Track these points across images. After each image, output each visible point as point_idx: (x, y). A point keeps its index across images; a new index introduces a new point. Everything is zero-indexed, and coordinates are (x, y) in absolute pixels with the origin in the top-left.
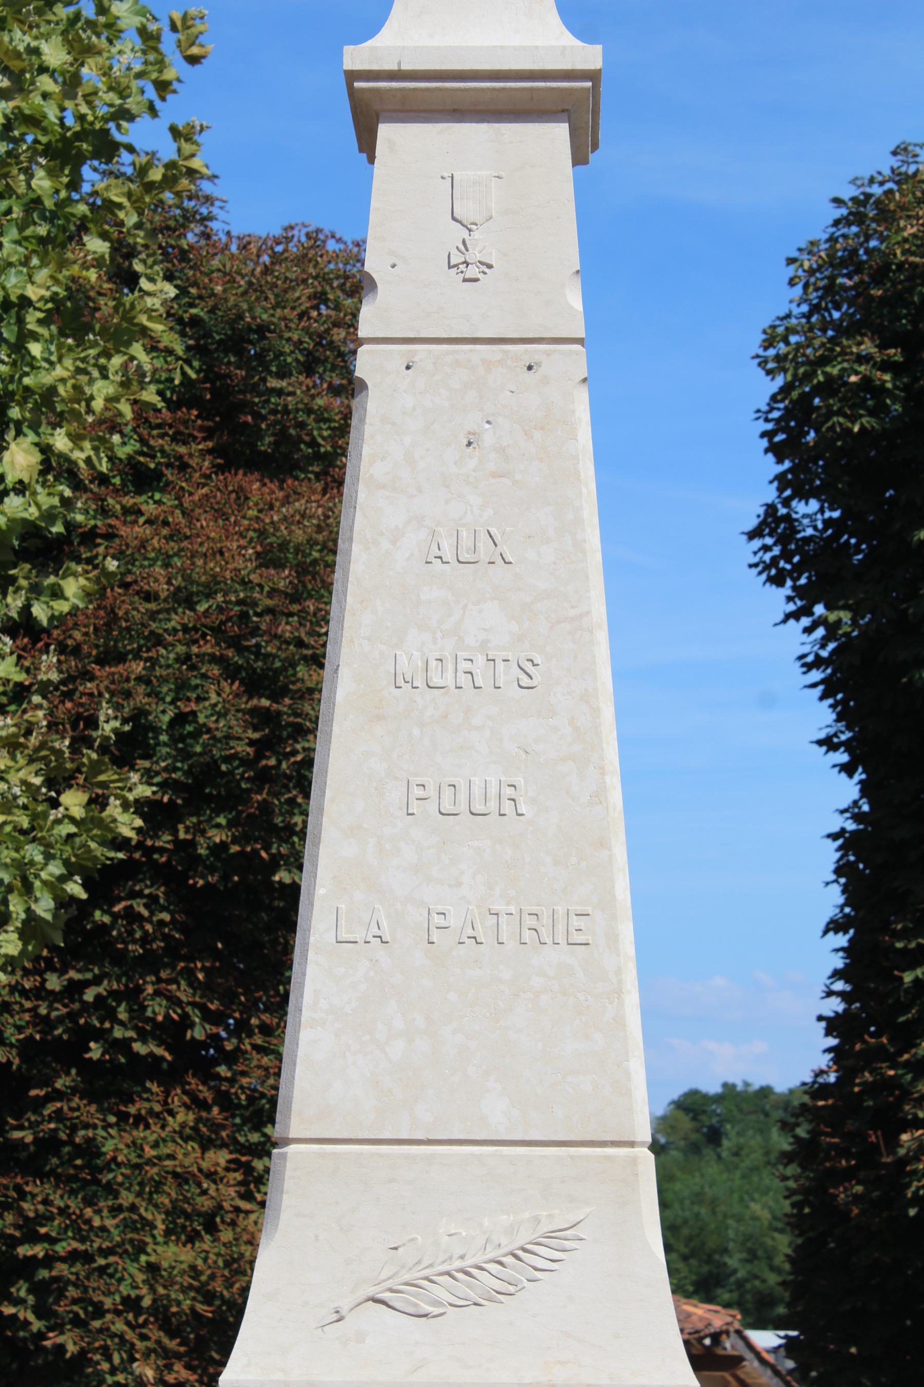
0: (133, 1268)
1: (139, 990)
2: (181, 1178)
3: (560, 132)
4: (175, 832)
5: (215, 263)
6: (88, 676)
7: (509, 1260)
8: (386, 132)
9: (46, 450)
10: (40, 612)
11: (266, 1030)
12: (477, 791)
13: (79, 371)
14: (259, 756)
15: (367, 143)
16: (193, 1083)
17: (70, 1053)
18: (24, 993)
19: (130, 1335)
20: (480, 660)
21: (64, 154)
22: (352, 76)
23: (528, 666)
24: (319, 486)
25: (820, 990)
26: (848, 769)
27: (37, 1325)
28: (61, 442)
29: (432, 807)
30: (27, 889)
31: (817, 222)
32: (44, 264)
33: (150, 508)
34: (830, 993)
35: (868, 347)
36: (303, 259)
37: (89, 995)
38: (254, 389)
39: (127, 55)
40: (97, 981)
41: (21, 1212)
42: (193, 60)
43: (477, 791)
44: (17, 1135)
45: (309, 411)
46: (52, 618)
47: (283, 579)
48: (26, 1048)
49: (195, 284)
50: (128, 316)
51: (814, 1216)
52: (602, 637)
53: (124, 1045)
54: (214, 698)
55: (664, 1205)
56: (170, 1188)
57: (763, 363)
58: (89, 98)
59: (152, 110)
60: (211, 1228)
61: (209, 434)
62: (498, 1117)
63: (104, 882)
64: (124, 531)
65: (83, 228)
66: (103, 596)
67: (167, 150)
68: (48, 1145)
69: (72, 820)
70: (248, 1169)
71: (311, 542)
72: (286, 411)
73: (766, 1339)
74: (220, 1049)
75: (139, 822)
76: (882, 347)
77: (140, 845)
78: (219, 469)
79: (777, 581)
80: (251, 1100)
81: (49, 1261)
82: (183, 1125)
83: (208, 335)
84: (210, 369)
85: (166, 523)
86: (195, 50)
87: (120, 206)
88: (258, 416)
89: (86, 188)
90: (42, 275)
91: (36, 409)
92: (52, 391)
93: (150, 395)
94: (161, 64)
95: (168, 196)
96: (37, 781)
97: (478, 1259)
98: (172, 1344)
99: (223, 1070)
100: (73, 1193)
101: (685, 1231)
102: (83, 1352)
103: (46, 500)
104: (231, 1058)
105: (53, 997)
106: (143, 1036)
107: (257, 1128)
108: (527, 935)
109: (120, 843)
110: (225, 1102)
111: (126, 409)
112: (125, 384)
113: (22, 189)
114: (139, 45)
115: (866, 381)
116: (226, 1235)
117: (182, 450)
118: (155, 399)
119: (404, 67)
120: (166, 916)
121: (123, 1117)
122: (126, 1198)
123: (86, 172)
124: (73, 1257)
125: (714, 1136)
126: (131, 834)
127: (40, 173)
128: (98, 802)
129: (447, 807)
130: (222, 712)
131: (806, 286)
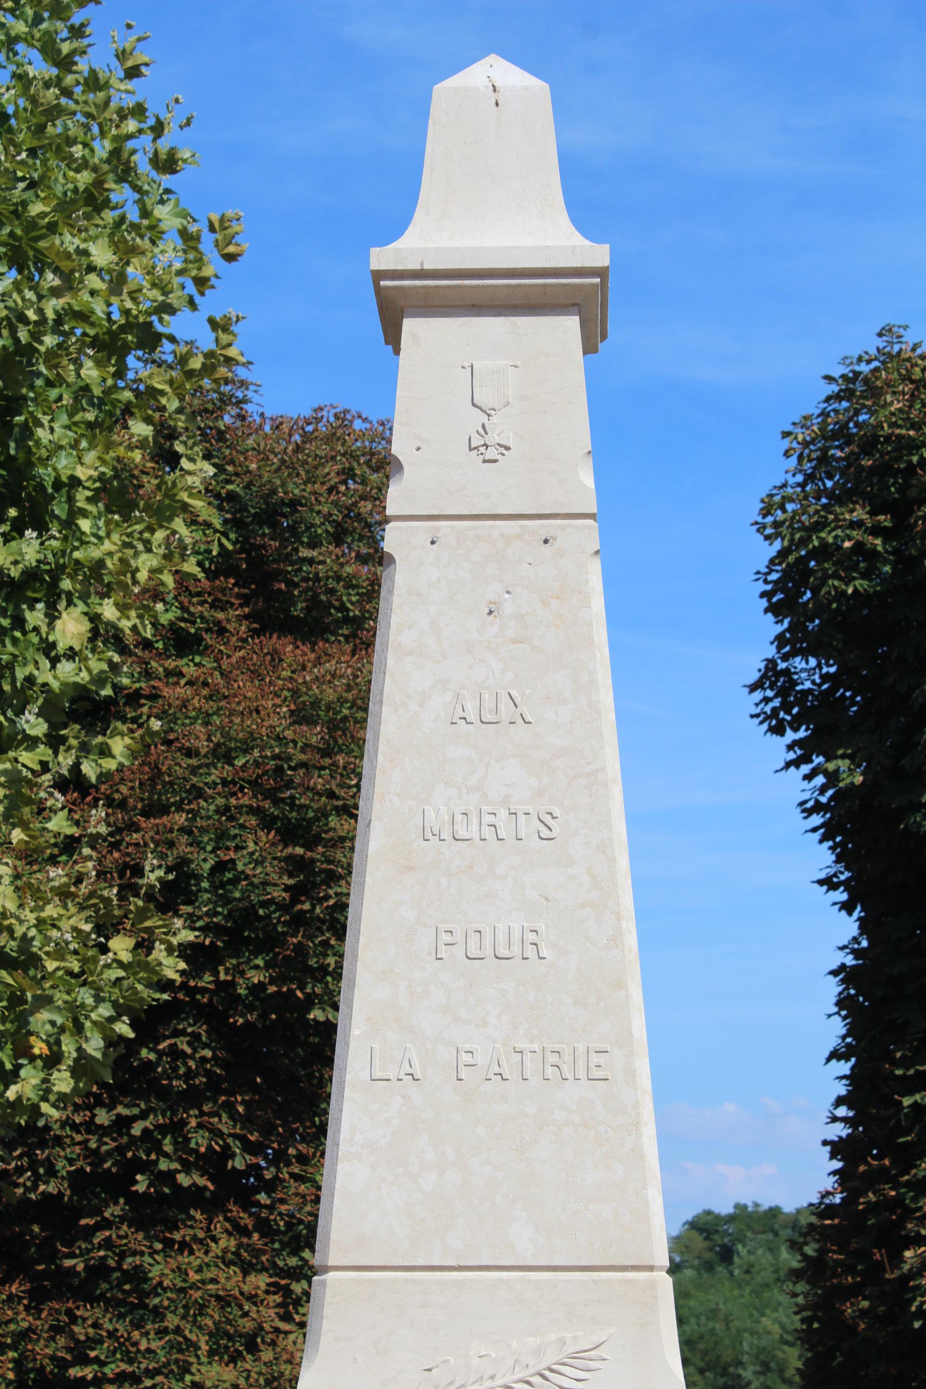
1: (183, 1123)
2: (224, 1301)
3: (571, 324)
4: (216, 973)
5: (250, 442)
6: (133, 827)
7: (537, 1380)
8: (410, 326)
9: (94, 618)
10: (89, 770)
11: (303, 1159)
12: (501, 937)
13: (126, 545)
14: (295, 900)
15: (393, 337)
16: (235, 1210)
17: (119, 1184)
18: (75, 1127)
20: (503, 813)
21: (110, 346)
22: (378, 276)
23: (548, 819)
24: (348, 648)
25: (824, 1115)
26: (847, 907)
28: (109, 611)
29: (459, 952)
30: (79, 1029)
31: (811, 397)
32: (92, 447)
33: (190, 671)
34: (834, 1119)
35: (860, 513)
36: (331, 438)
37: (136, 1130)
38: (287, 558)
39: (169, 254)
40: (143, 1116)
41: (72, 1336)
42: (230, 258)
43: (501, 937)
44: (68, 1263)
45: (338, 578)
46: (100, 776)
47: (315, 735)
48: (76, 1179)
49: (232, 462)
50: (170, 494)
52: (617, 791)
53: (170, 1176)
54: (251, 846)
55: (680, 1321)
56: (214, 1311)
57: (761, 528)
58: (134, 295)
59: (192, 303)
60: (252, 1348)
61: (246, 600)
62: (525, 1244)
63: (150, 1022)
64: (166, 692)
65: (128, 411)
66: (148, 754)
67: (206, 340)
68: (99, 1271)
69: (121, 964)
70: (286, 1291)
71: (342, 701)
72: (317, 579)
74: (260, 1178)
75: (182, 965)
76: (872, 513)
77: (184, 985)
78: (256, 633)
79: (778, 730)
80: (290, 1226)
82: (225, 1251)
83: (244, 509)
84: (246, 540)
85: (205, 684)
86: (231, 249)
87: (162, 393)
88: (291, 584)
89: (131, 375)
90: (91, 457)
91: (86, 581)
92: (101, 563)
93: (191, 566)
94: (199, 261)
95: (206, 383)
96: (87, 927)
99: (262, 1198)
100: (121, 1316)
101: (702, 1346)
103: (97, 666)
104: (270, 1186)
105: (103, 1131)
106: (187, 1168)
107: (295, 1252)
108: (550, 1072)
109: (165, 985)
110: (264, 1227)
111: (169, 580)
112: (168, 557)
113: (71, 378)
114: (180, 245)
115: (859, 547)
116: (267, 1355)
117: (221, 616)
118: (196, 570)
119: (427, 266)
120: (208, 1053)
121: (168, 1243)
122: (172, 1320)
123: (131, 361)
125: (726, 1255)
126: (176, 977)
127: (88, 364)
128: (144, 946)
129: (473, 951)
130: (259, 859)
131: (800, 458)
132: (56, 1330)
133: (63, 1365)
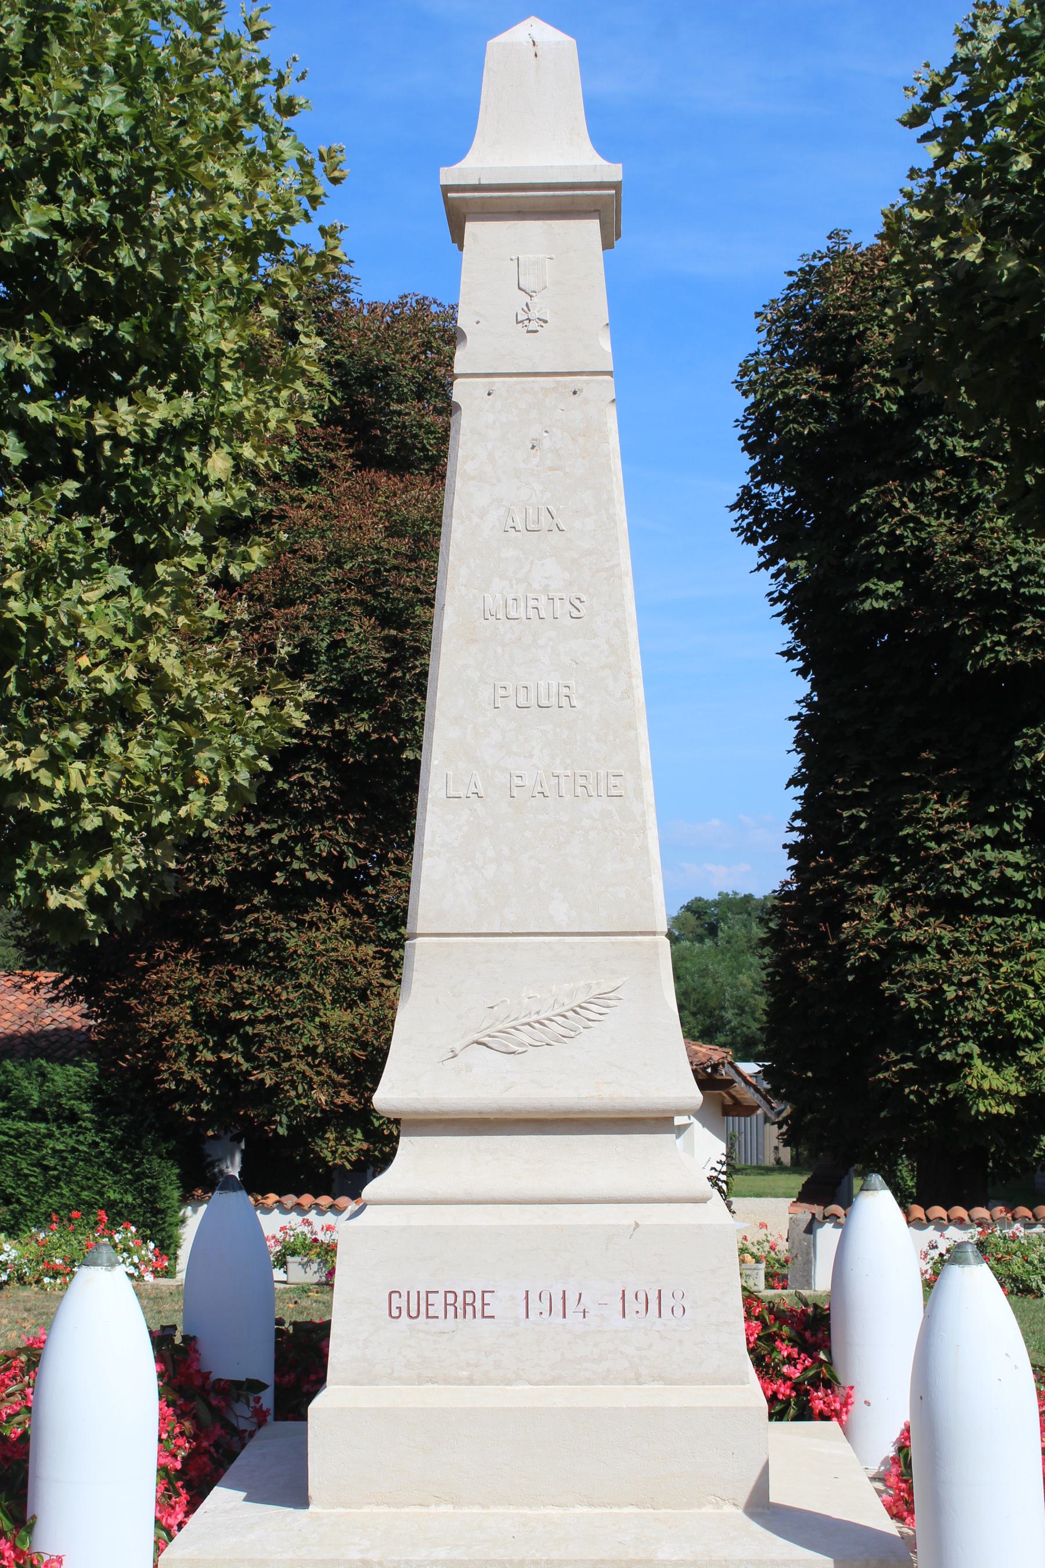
0: (310, 1027)
2: (342, 964)
7: (570, 1014)
19: (309, 1072)
27: (245, 1066)
41: (232, 989)
44: (228, 937)
51: (782, 983)
56: (335, 971)
68: (250, 943)
73: (749, 1068)
81: (252, 1022)
82: (343, 928)
97: (548, 1014)
98: (338, 1078)
102: (277, 1084)
121: (301, 923)
122: (305, 979)
124: (268, 1020)
125: (713, 930)
132: (220, 985)
133: (227, 1010)
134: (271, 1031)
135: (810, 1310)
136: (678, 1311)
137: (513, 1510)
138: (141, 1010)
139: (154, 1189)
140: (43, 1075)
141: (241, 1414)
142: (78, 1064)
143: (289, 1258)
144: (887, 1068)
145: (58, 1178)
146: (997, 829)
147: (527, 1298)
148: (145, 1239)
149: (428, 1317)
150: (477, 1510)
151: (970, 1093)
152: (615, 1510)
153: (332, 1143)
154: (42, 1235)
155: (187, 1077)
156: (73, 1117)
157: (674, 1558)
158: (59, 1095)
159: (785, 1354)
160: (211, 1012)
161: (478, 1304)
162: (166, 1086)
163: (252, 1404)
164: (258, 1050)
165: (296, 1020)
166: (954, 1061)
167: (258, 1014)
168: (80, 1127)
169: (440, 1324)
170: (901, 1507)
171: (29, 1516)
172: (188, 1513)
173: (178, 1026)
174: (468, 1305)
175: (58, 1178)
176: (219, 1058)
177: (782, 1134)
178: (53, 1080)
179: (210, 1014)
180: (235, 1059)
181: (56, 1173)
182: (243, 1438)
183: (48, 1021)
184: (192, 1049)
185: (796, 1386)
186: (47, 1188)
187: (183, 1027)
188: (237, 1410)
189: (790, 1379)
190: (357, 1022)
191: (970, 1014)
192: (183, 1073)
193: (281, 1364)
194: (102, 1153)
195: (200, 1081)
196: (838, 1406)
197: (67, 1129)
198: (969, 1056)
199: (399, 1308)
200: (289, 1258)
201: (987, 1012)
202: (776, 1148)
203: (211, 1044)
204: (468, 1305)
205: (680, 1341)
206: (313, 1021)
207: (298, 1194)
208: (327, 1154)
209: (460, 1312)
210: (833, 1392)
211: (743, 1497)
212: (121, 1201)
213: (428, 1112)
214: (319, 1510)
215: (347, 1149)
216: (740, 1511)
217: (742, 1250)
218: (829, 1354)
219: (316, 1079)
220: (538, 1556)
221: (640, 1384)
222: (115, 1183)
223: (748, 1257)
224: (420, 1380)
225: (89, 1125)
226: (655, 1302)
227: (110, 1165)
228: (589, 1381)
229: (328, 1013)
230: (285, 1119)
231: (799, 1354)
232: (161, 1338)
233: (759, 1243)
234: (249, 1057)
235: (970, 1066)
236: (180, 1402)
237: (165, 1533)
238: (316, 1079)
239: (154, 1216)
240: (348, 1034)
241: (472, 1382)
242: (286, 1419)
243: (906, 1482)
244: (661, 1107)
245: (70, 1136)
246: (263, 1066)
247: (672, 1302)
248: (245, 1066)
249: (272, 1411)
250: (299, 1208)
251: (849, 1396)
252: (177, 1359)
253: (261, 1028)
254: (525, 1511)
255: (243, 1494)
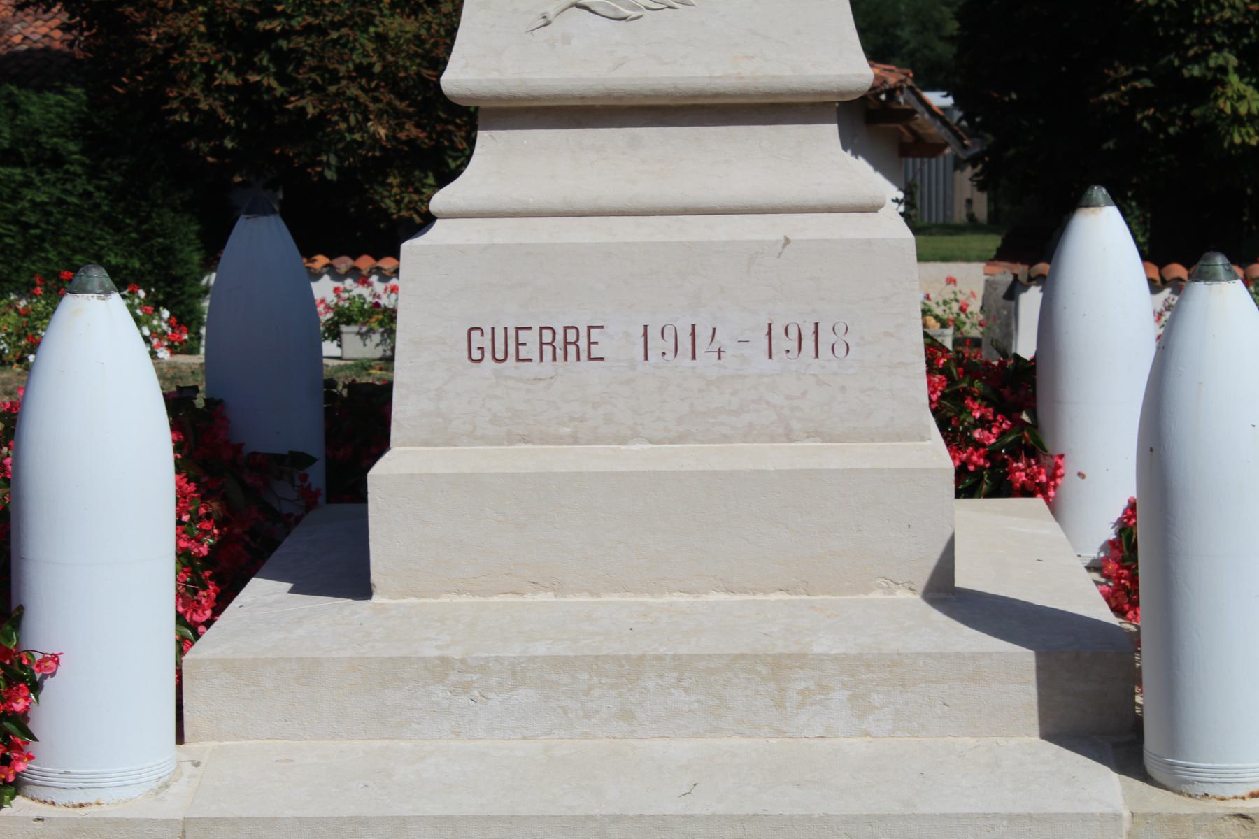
0: (363, 39)
19: (363, 98)
27: (280, 91)
73: (937, 99)
81: (287, 33)
98: (401, 105)
102: (322, 114)
124: (308, 30)
133: (252, 18)
134: (312, 46)
135: (1010, 363)
136: (840, 350)
137: (630, 598)
138: (139, 17)
139: (167, 251)
140: (14, 105)
141: (284, 495)
142: (60, 91)
143: (344, 328)
144: (1114, 87)
145: (42, 239)
146: (1240, 47)
147: (645, 334)
148: (157, 306)
149: (518, 360)
150: (584, 598)
151: (1223, 119)
152: (760, 597)
153: (395, 190)
154: (23, 303)
155: (204, 106)
156: (57, 160)
157: (833, 652)
158: (37, 132)
159: (978, 415)
160: (232, 21)
161: (583, 343)
162: (177, 118)
163: (298, 483)
164: (296, 70)
165: (344, 31)
166: (1203, 77)
167: (294, 23)
168: (67, 172)
169: (533, 368)
170: (1123, 596)
171: (14, 606)
172: (218, 610)
173: (189, 39)
174: (570, 344)
175: (42, 239)
176: (246, 81)
177: (976, 175)
178: (28, 113)
179: (231, 22)
180: (265, 82)
181: (38, 231)
182: (289, 523)
183: (17, 39)
184: (209, 70)
185: (991, 455)
186: (28, 252)
187: (195, 42)
188: (276, 493)
189: (984, 446)
190: (423, 32)
191: (1227, 13)
192: (198, 101)
193: (331, 438)
194: (97, 206)
195: (220, 111)
196: (1043, 478)
197: (50, 175)
198: (1223, 70)
199: (481, 349)
200: (344, 328)
201: (1248, 12)
202: (969, 202)
203: (234, 63)
204: (570, 344)
205: (843, 389)
206: (366, 31)
207: (355, 256)
208: (389, 204)
209: (560, 353)
210: (1038, 462)
211: (922, 579)
212: (126, 267)
213: (513, 98)
214: (384, 601)
215: (415, 197)
216: (917, 598)
217: (925, 312)
218: (1033, 414)
219: (372, 106)
220: (662, 650)
221: (791, 440)
222: (116, 243)
223: (931, 321)
224: (511, 439)
225: (79, 170)
226: (809, 339)
227: (108, 220)
228: (726, 439)
229: (386, 21)
230: (333, 160)
231: (997, 417)
232: (179, 403)
233: (945, 303)
234: (283, 79)
235: (1224, 84)
236: (204, 479)
237: (190, 628)
238: (372, 106)
239: (169, 285)
240: (413, 48)
241: (575, 440)
242: (342, 501)
243: (1127, 568)
244: (819, 88)
245: (54, 184)
246: (303, 90)
247: (833, 338)
248: (280, 91)
249: (323, 492)
250: (355, 274)
251: (1058, 467)
252: (201, 429)
253: (299, 42)
254: (648, 599)
255: (289, 586)
